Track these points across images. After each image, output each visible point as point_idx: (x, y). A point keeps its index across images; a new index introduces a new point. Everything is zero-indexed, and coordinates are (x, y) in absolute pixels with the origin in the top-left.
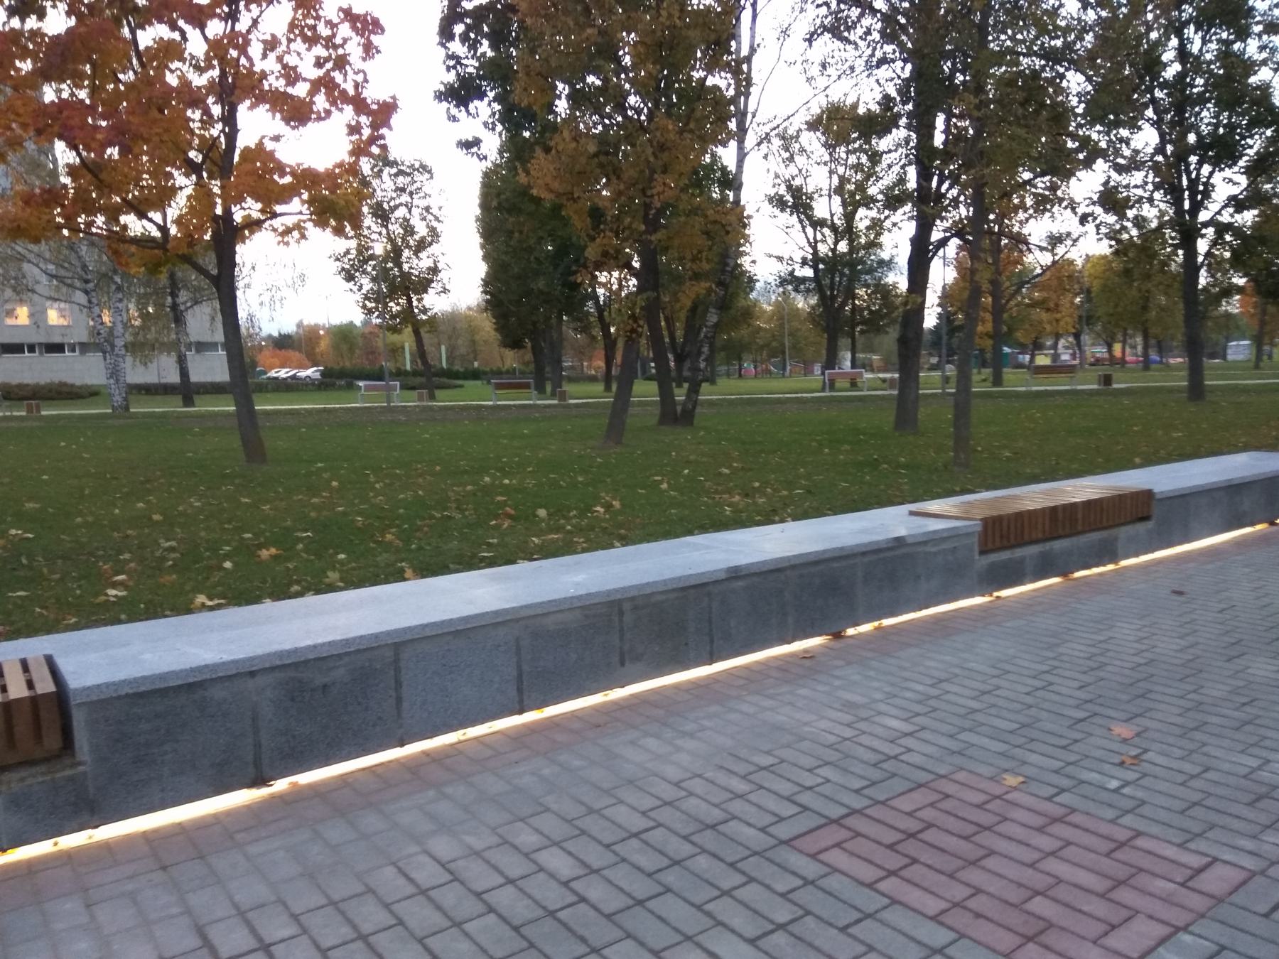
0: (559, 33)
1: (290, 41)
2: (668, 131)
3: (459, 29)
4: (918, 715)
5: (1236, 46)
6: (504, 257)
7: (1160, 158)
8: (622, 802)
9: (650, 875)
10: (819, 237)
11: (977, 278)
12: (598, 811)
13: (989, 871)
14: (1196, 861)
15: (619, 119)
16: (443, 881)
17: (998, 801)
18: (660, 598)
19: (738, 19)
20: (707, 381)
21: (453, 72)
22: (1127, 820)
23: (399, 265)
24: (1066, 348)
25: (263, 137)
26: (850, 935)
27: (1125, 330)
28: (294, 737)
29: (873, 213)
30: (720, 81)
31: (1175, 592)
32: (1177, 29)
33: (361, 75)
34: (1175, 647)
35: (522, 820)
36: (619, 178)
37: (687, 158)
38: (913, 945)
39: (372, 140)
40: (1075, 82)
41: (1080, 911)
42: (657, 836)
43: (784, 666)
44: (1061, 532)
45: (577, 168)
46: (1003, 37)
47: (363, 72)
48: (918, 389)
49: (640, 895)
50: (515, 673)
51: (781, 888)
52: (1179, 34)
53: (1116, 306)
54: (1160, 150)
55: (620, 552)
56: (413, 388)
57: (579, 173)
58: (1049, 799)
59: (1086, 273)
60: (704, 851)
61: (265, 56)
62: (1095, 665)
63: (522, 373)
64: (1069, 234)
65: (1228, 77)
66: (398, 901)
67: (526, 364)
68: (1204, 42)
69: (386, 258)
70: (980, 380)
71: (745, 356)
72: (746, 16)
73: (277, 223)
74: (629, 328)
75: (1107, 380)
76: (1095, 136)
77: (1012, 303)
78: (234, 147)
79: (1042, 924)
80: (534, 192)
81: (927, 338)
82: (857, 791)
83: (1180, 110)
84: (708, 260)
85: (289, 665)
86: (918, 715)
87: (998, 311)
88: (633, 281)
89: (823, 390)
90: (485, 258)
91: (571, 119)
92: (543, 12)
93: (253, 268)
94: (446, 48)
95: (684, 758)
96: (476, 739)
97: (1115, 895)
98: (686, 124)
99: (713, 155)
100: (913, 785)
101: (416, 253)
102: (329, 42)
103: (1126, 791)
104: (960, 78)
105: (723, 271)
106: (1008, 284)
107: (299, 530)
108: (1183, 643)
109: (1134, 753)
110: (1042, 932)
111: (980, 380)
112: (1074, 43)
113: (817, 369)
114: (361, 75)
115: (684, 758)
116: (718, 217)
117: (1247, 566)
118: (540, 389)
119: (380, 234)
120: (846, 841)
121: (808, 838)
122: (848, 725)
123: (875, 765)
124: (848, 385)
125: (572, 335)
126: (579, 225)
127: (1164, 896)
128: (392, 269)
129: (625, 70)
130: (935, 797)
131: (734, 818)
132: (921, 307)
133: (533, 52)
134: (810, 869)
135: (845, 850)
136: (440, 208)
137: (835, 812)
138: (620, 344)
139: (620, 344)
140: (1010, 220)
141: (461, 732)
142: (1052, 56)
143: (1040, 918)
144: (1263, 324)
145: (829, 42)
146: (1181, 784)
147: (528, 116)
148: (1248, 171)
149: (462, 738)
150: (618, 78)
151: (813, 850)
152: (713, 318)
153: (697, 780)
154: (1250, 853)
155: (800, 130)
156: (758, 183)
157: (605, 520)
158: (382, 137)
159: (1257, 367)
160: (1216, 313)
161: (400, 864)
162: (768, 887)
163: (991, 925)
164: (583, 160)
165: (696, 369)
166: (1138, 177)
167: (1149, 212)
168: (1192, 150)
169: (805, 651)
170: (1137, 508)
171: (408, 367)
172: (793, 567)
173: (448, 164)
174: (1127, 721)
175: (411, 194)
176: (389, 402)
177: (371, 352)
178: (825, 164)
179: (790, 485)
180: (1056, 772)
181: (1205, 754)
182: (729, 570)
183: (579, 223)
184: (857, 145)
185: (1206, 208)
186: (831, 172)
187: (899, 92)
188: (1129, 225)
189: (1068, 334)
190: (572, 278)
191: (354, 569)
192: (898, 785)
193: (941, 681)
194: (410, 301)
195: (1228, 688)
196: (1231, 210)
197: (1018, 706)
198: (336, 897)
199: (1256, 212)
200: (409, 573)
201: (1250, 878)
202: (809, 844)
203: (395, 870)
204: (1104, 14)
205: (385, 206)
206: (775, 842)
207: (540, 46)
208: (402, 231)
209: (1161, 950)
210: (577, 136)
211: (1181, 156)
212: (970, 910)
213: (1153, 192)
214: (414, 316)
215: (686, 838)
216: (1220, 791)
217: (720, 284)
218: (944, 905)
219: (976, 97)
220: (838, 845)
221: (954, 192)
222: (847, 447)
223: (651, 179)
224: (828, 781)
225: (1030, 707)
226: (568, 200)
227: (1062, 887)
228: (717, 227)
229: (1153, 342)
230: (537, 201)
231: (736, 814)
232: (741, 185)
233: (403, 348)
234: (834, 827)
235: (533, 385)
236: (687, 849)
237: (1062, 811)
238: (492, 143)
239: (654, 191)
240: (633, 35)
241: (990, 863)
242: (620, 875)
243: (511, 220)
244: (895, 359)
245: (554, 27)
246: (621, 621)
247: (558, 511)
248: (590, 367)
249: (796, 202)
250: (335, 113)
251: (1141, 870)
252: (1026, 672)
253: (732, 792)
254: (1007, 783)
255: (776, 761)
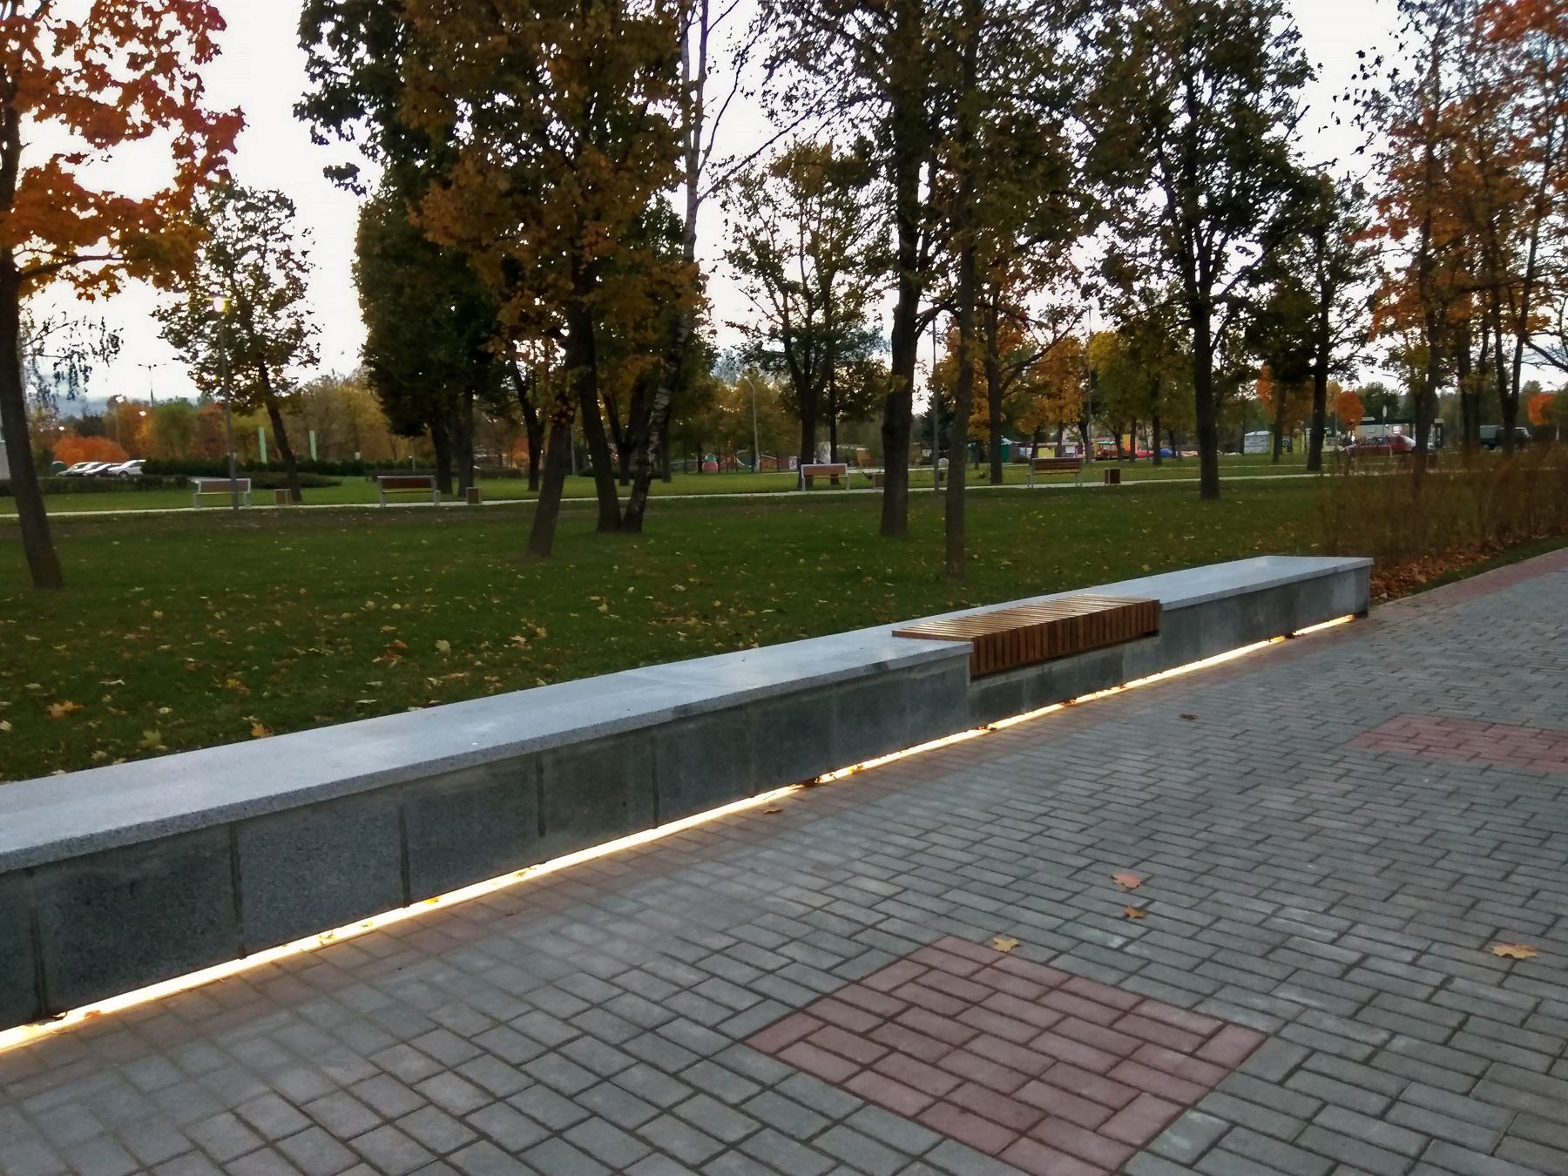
0: (459, 39)
1: (94, 32)
2: (600, 168)
3: (327, 27)
4: (900, 873)
5: (1248, 98)
6: (390, 318)
7: (1168, 223)
8: (536, 1008)
9: (570, 1098)
10: (790, 304)
11: (967, 357)
12: (506, 1023)
13: (977, 1055)
14: (1205, 1026)
15: (540, 150)
16: (297, 1127)
17: (988, 970)
18: (592, 747)
19: (684, 35)
20: (659, 477)
21: (320, 82)
22: (1132, 984)
23: (248, 325)
24: (1071, 439)
25: (57, 156)
26: (815, 1149)
27: (1134, 419)
28: (90, 952)
29: (852, 279)
30: (661, 108)
31: (1184, 717)
32: (1184, 74)
33: (194, 81)
34: (1183, 779)
35: (404, 1042)
36: (539, 223)
37: (624, 201)
38: (888, 1152)
39: (209, 164)
40: (1075, 130)
41: (1079, 1095)
42: (580, 1048)
43: (745, 823)
44: (1060, 652)
45: (486, 209)
46: (994, 75)
47: (196, 76)
48: (906, 487)
49: (557, 1124)
50: (398, 853)
51: (733, 1098)
52: (1188, 82)
53: (1124, 392)
54: (1169, 213)
55: (544, 691)
56: (270, 487)
57: (489, 215)
58: (1045, 964)
59: (1091, 354)
60: (641, 1061)
61: (58, 51)
62: (1098, 803)
63: (419, 466)
64: (1071, 309)
65: (1240, 133)
66: (236, 1158)
67: (426, 455)
68: (1215, 92)
69: (231, 317)
70: (975, 477)
71: (705, 446)
72: (694, 33)
73: (78, 270)
74: (557, 410)
75: (1114, 476)
76: (1097, 196)
77: (1011, 387)
78: (16, 168)
79: (1037, 1115)
80: (429, 236)
81: (916, 428)
82: (828, 971)
83: (1190, 170)
84: (655, 330)
85: (82, 857)
86: (900, 873)
87: (995, 396)
88: (562, 352)
89: (799, 488)
90: (366, 319)
91: (478, 147)
92: (437, 13)
93: (46, 329)
94: (310, 51)
95: (619, 947)
96: (346, 942)
97: (1120, 1073)
98: (624, 160)
99: (660, 201)
100: (893, 958)
101: (272, 311)
102: (148, 36)
103: (1130, 949)
104: (945, 122)
105: (675, 343)
106: (1006, 365)
107: (105, 677)
108: (1192, 774)
109: (1138, 905)
110: (1037, 1124)
111: (975, 477)
112: (1072, 86)
113: (793, 462)
114: (194, 81)
115: (619, 947)
116: (665, 277)
117: (1262, 685)
118: (445, 488)
119: (222, 285)
120: (812, 1032)
121: (767, 1034)
122: (820, 892)
123: (849, 938)
124: (828, 482)
125: (486, 418)
126: (489, 280)
127: (1171, 1070)
128: (238, 331)
129: (544, 89)
130: (917, 970)
131: (679, 1016)
132: (908, 389)
133: (424, 60)
134: (767, 1069)
135: (810, 1043)
136: (304, 253)
137: (800, 997)
138: (548, 432)
139: (548, 432)
140: (1006, 290)
141: (325, 934)
142: (1043, 97)
143: (1033, 1107)
144: (1281, 412)
145: (795, 71)
146: (1190, 938)
147: (420, 140)
148: (1263, 239)
149: (326, 942)
150: (536, 98)
151: (772, 1048)
152: (663, 400)
153: (635, 973)
154: (1263, 1012)
155: (764, 175)
156: (713, 237)
157: (526, 653)
158: (224, 161)
159: (1276, 460)
160: (1231, 400)
161: (239, 1110)
162: (718, 1099)
163: (980, 1121)
164: (492, 198)
165: (643, 463)
166: (1145, 244)
167: (1157, 284)
168: (1203, 214)
169: (772, 804)
170: (1142, 622)
171: (264, 459)
172: (757, 703)
173: (314, 195)
174: (1130, 867)
175: (265, 234)
176: (236, 504)
177: (212, 439)
178: (796, 217)
179: (758, 603)
180: (1053, 931)
181: (1216, 902)
182: (678, 709)
183: (490, 278)
184: (831, 196)
185: (1219, 281)
186: (803, 227)
187: (877, 134)
188: (1136, 298)
189: (1073, 424)
190: (481, 347)
191: (181, 726)
192: (876, 959)
193: (927, 831)
194: (264, 372)
195: (1241, 825)
196: (1245, 283)
197: (1013, 856)
198: (150, 1161)
199: (1272, 286)
200: (258, 729)
201: (1262, 1042)
202: (769, 1041)
203: (232, 1118)
204: (1105, 53)
205: (229, 249)
206: (728, 1041)
207: (434, 54)
208: (251, 282)
209: (1167, 1132)
210: (483, 169)
211: (1192, 219)
212: (955, 1104)
213: (1161, 261)
214: (270, 392)
215: (618, 1047)
216: (1231, 943)
217: (671, 358)
218: (926, 1101)
219: (963, 144)
220: (803, 1039)
221: (944, 256)
222: (825, 556)
223: (581, 227)
224: (794, 961)
225: (1026, 856)
226: (474, 248)
227: (1061, 1068)
228: (665, 288)
229: (1163, 432)
230: (434, 248)
231: (682, 1011)
232: (694, 238)
233: (256, 434)
234: (799, 1017)
235: (434, 483)
236: (619, 1060)
237: (1060, 977)
238: (373, 174)
239: (585, 241)
240: (554, 46)
241: (978, 1045)
242: (533, 1102)
243: (400, 271)
244: (881, 451)
245: (451, 31)
246: (540, 780)
247: (466, 643)
248: (510, 459)
249: (761, 261)
250: (159, 130)
251: (1146, 1041)
252: (1021, 815)
253: (677, 984)
254: (999, 948)
255: (733, 941)
